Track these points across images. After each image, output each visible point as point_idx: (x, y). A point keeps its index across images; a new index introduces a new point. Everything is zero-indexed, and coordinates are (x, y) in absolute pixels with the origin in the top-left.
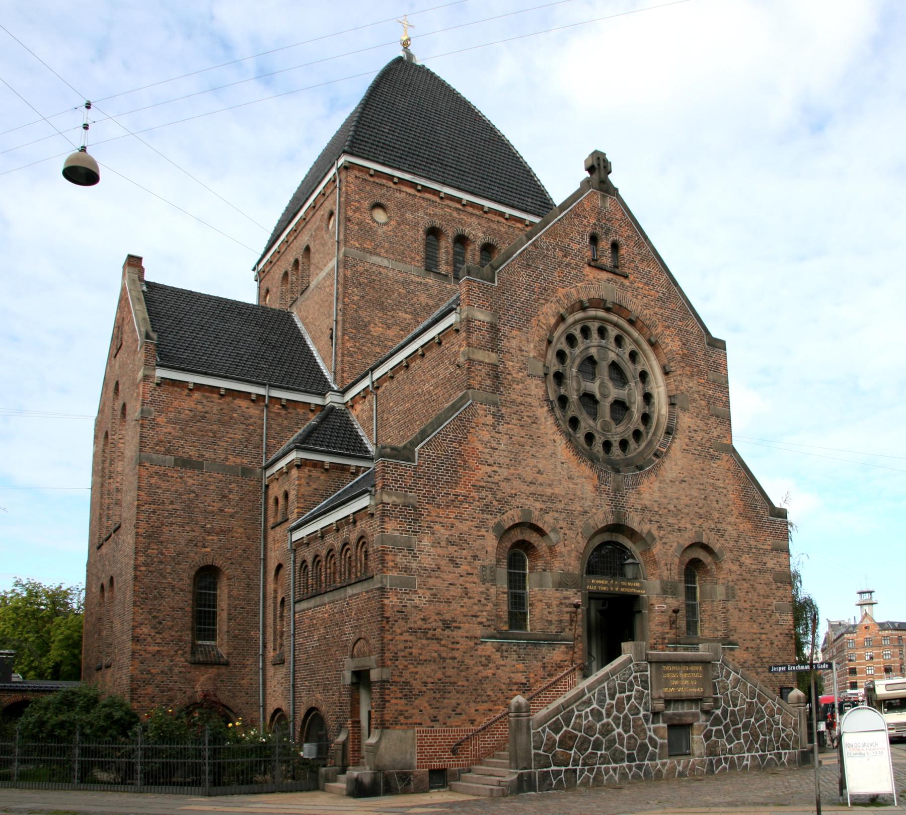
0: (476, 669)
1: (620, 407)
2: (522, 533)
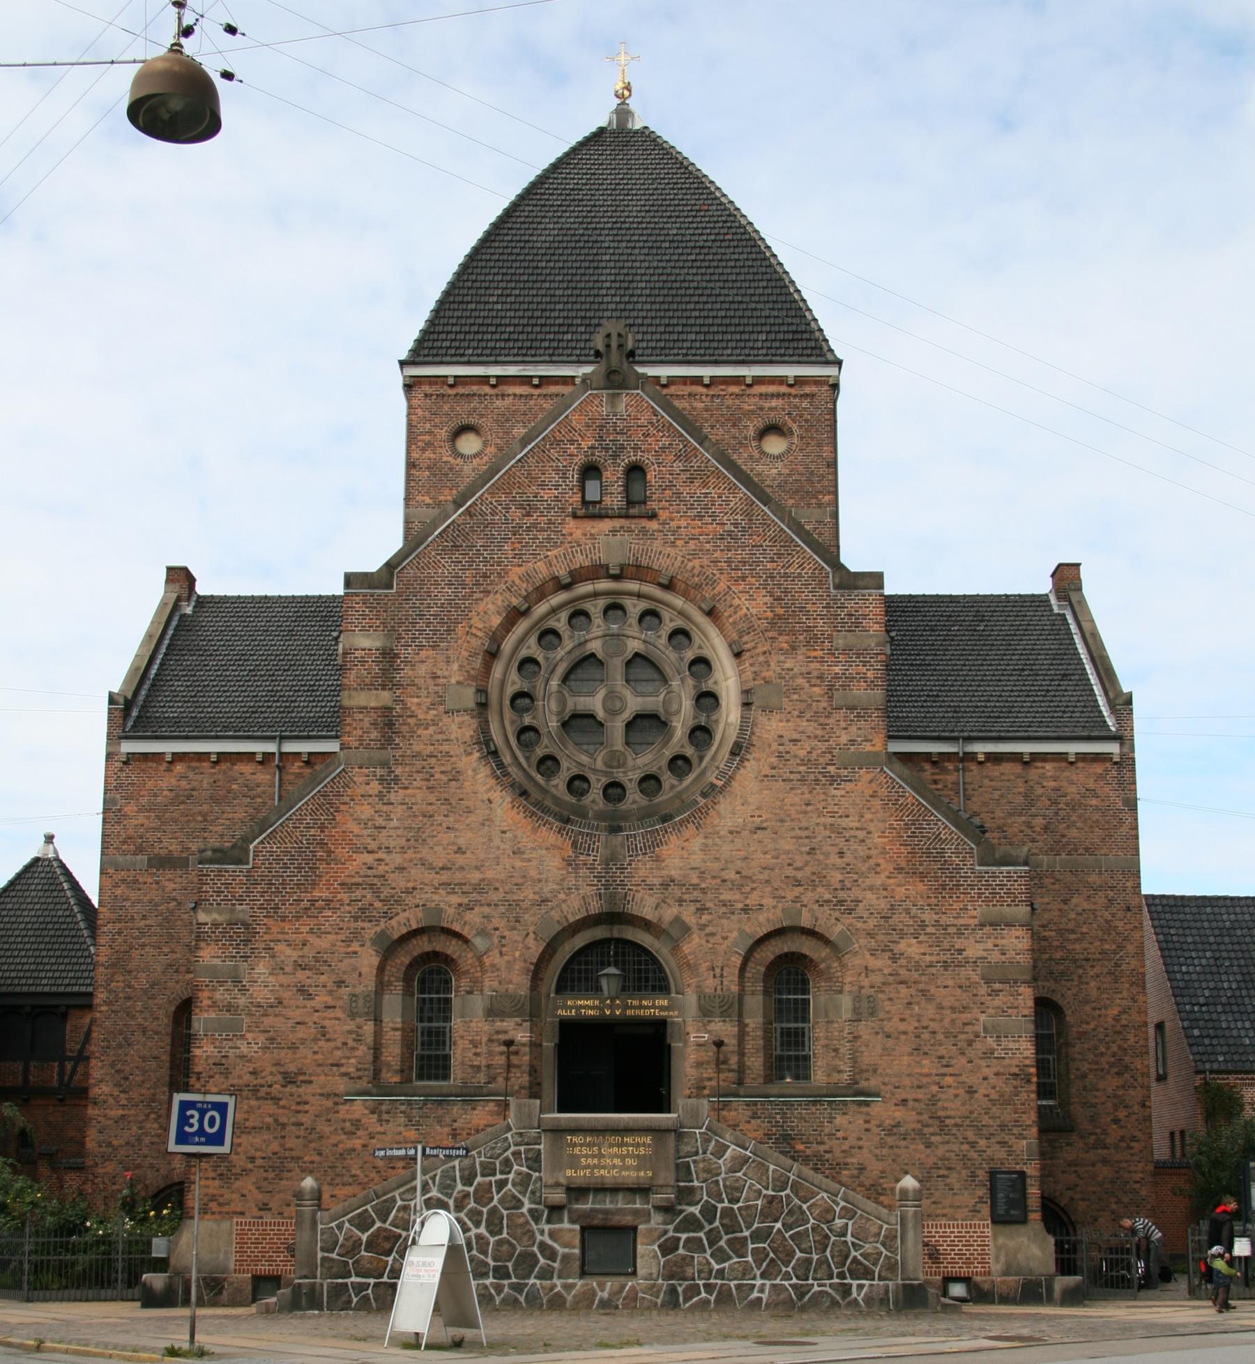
0: (333, 1140)
1: (648, 724)
2: (430, 941)
